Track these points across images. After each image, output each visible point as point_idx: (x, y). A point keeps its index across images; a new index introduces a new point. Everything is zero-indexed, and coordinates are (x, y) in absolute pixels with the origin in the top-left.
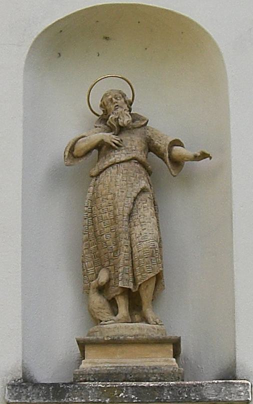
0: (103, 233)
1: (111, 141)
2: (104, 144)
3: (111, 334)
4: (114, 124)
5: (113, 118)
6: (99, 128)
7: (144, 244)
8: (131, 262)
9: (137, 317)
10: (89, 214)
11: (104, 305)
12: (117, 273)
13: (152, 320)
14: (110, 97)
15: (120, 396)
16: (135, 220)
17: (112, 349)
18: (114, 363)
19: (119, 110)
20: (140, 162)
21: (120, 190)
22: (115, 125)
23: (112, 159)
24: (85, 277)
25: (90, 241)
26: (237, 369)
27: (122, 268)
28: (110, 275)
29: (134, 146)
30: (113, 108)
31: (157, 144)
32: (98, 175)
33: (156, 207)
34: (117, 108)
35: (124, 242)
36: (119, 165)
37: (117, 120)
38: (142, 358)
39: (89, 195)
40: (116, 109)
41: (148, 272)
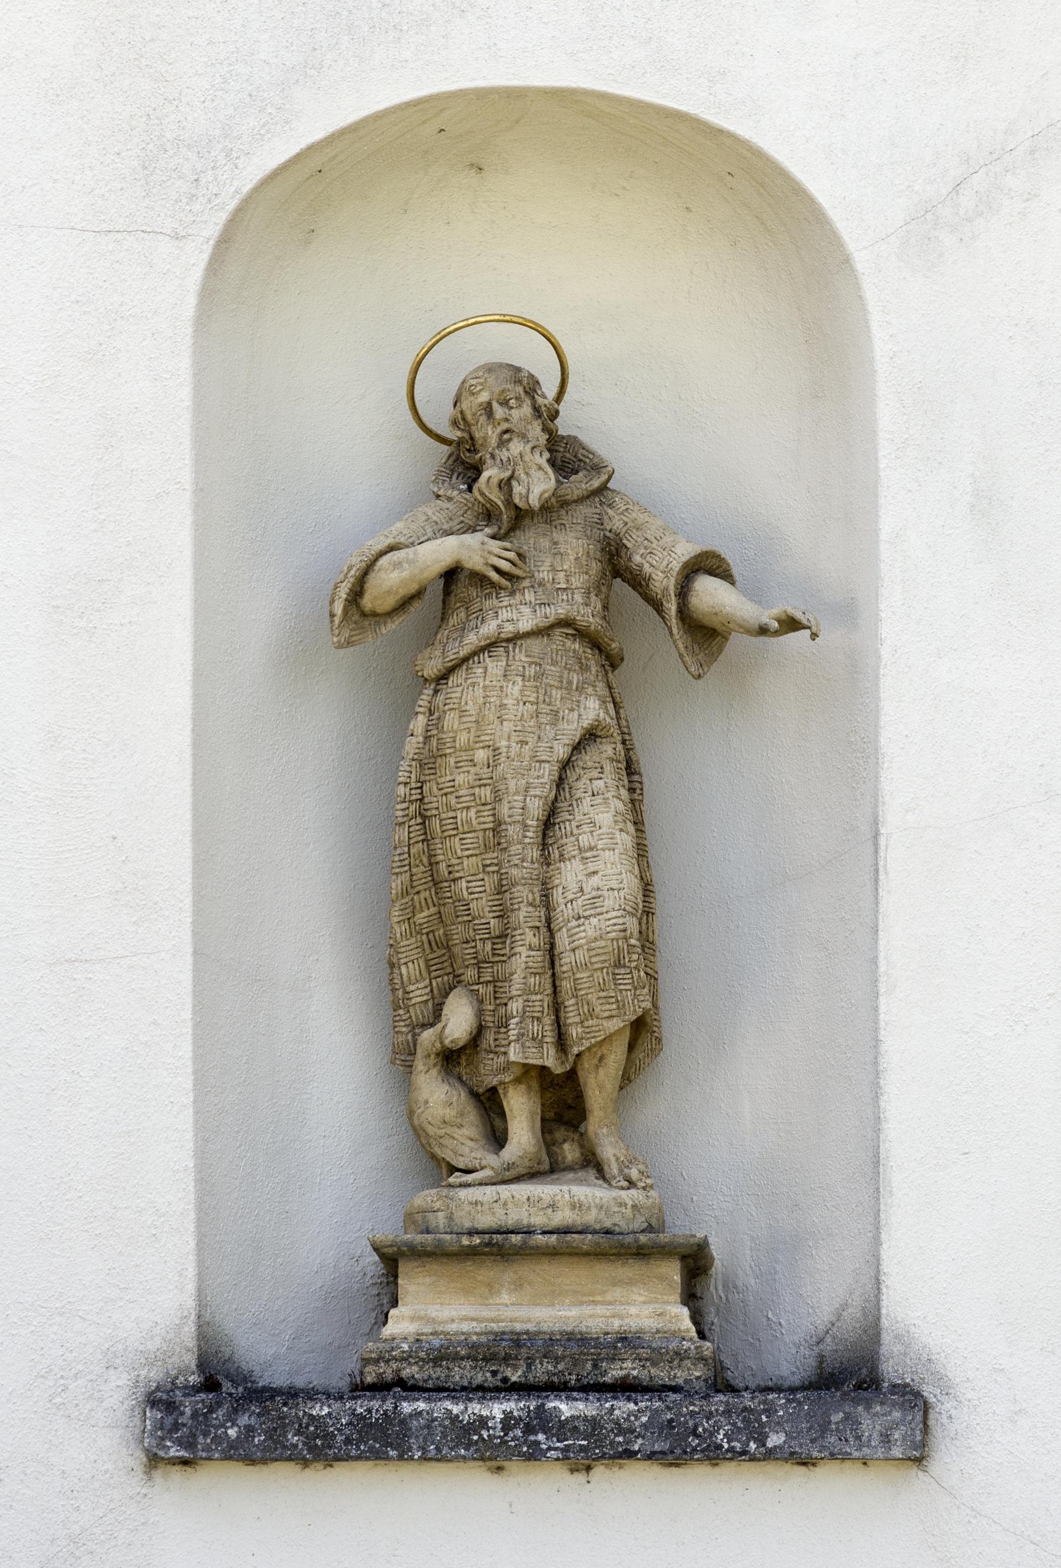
0: (457, 875)
1: (487, 564)
2: (458, 458)
3: (485, 1221)
4: (496, 500)
5: (495, 481)
6: (446, 505)
7: (590, 928)
8: (549, 981)
9: (570, 1152)
10: (412, 808)
11: (462, 1114)
12: (502, 1010)
13: (615, 1171)
14: (484, 397)
15: (486, 1438)
16: (564, 841)
17: (486, 1272)
18: (493, 1321)
19: (516, 447)
20: (582, 634)
21: (514, 738)
22: (500, 503)
23: (489, 628)
24: (401, 1012)
25: (418, 893)
26: (884, 1350)
27: (520, 1000)
28: (480, 1013)
29: (562, 575)
30: (493, 441)
31: (640, 566)
32: (443, 677)
33: (636, 778)
34: (510, 440)
35: (525, 915)
36: (511, 646)
37: (506, 485)
38: (582, 1303)
39: (411, 746)
40: (502, 443)
41: (606, 1014)
